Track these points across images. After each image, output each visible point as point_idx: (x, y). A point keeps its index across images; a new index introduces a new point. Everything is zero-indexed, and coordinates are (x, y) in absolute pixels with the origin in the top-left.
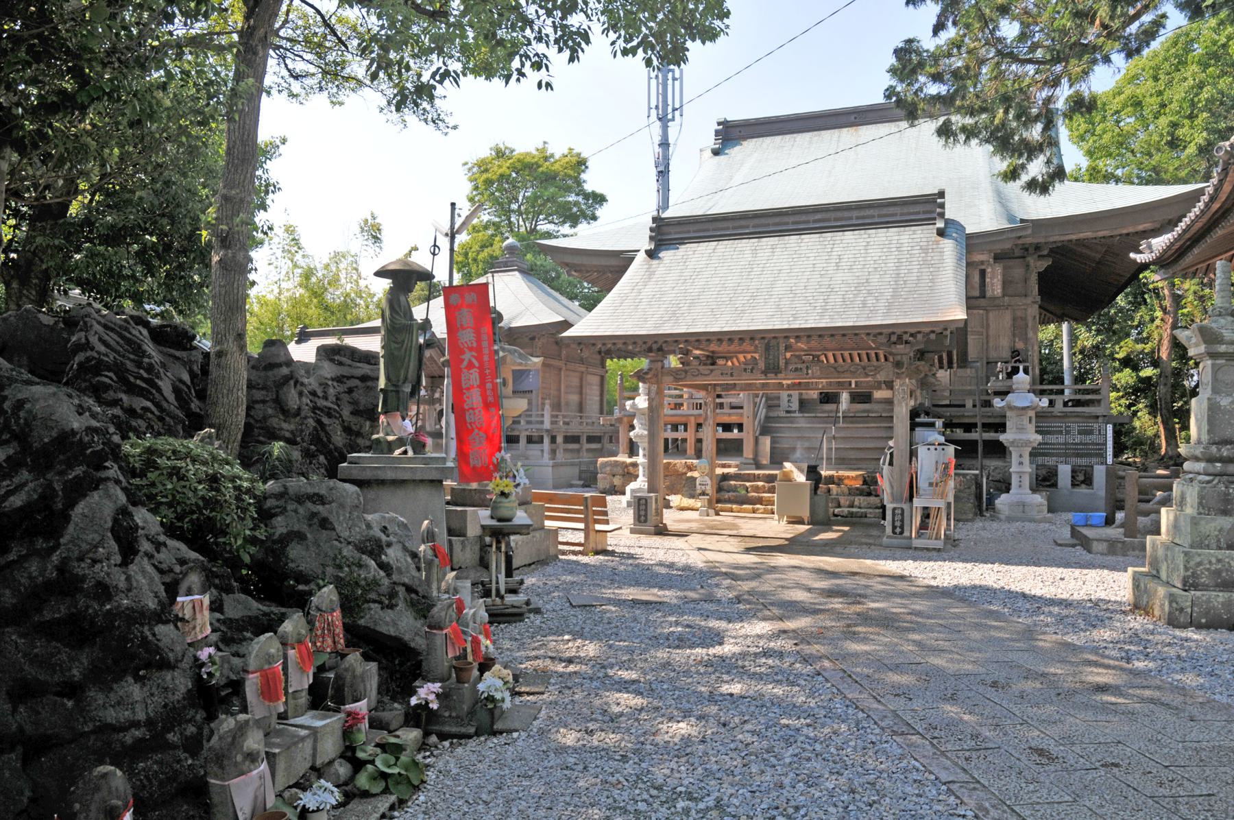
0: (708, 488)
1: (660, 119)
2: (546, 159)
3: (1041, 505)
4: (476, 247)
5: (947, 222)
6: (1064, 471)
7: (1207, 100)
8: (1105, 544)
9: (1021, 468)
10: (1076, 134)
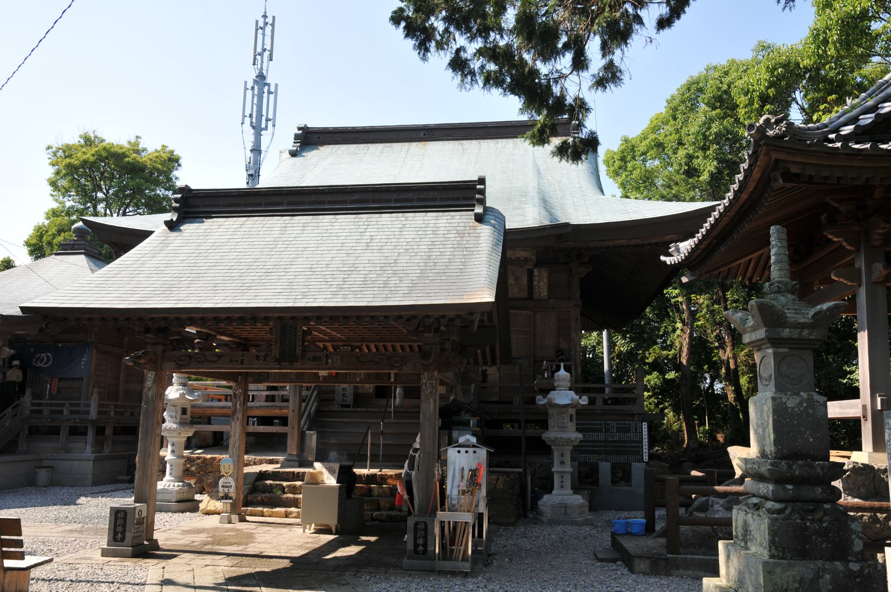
0: (231, 490)
1: (253, 127)
2: (137, 152)
3: (582, 506)
4: (53, 230)
5: (486, 209)
6: (605, 468)
7: (716, 133)
8: (647, 562)
9: (562, 467)
10: (612, 169)
